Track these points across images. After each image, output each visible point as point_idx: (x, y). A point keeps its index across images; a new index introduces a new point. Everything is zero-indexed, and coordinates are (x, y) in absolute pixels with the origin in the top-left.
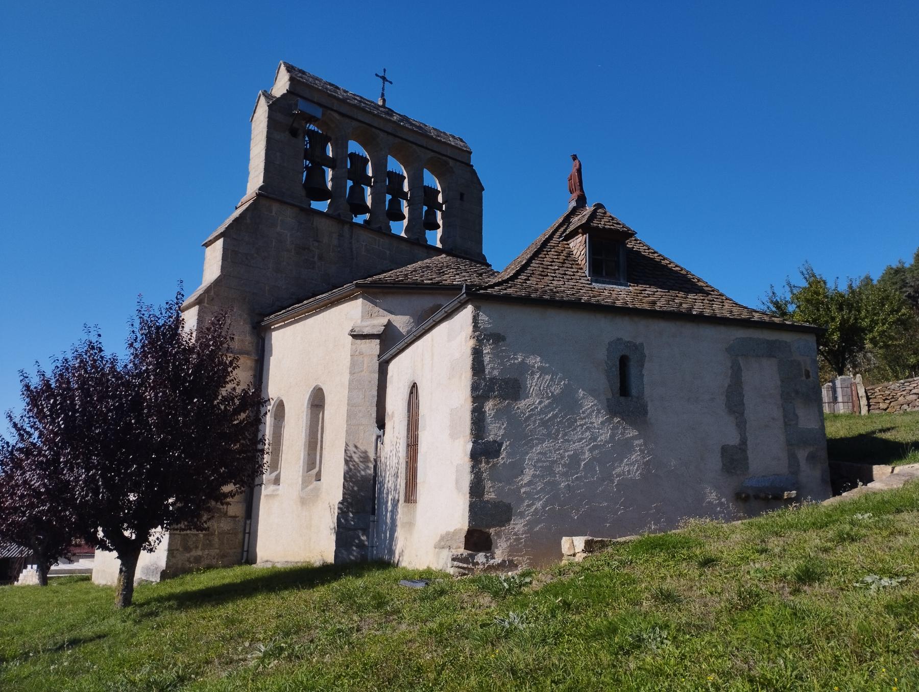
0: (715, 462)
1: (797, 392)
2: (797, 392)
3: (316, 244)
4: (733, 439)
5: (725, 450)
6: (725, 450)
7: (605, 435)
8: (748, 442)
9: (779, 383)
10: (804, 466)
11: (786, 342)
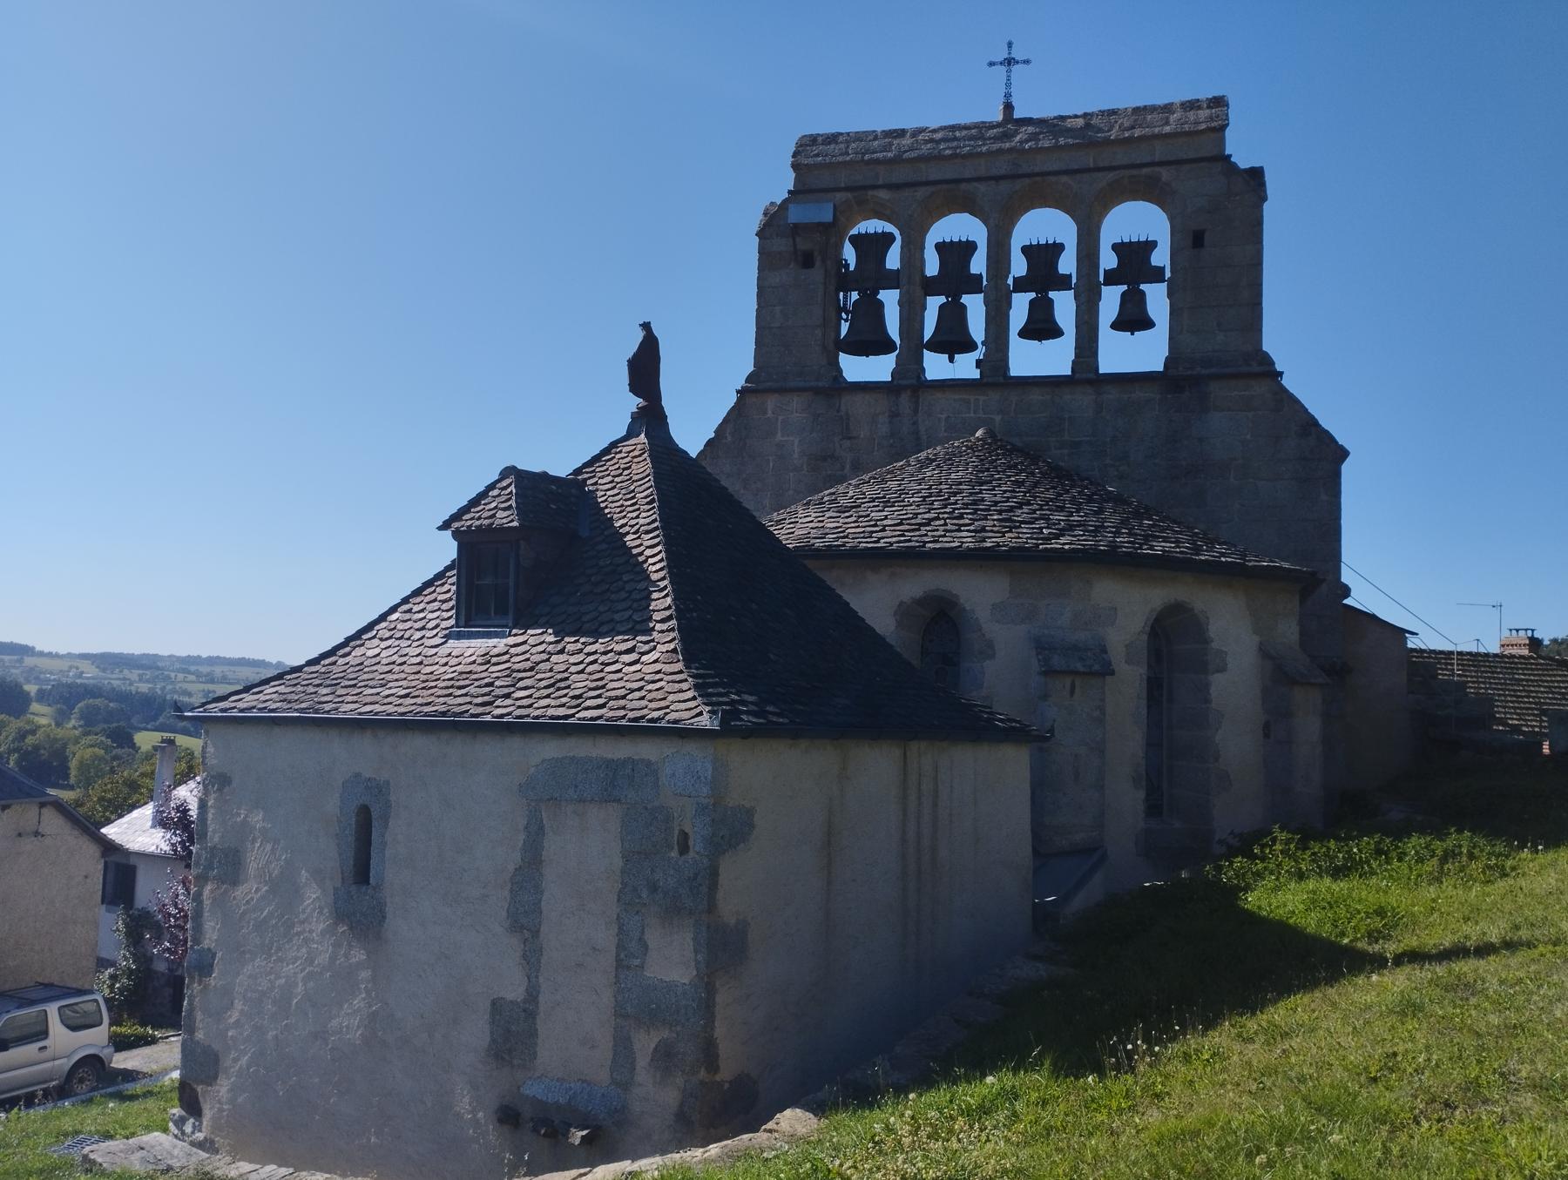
0: (476, 1032)
1: (654, 888)
2: (654, 888)
3: (847, 443)
4: (513, 990)
5: (497, 1006)
6: (497, 1006)
7: (323, 959)
8: (541, 998)
9: (618, 862)
10: (643, 1075)
11: (649, 764)
